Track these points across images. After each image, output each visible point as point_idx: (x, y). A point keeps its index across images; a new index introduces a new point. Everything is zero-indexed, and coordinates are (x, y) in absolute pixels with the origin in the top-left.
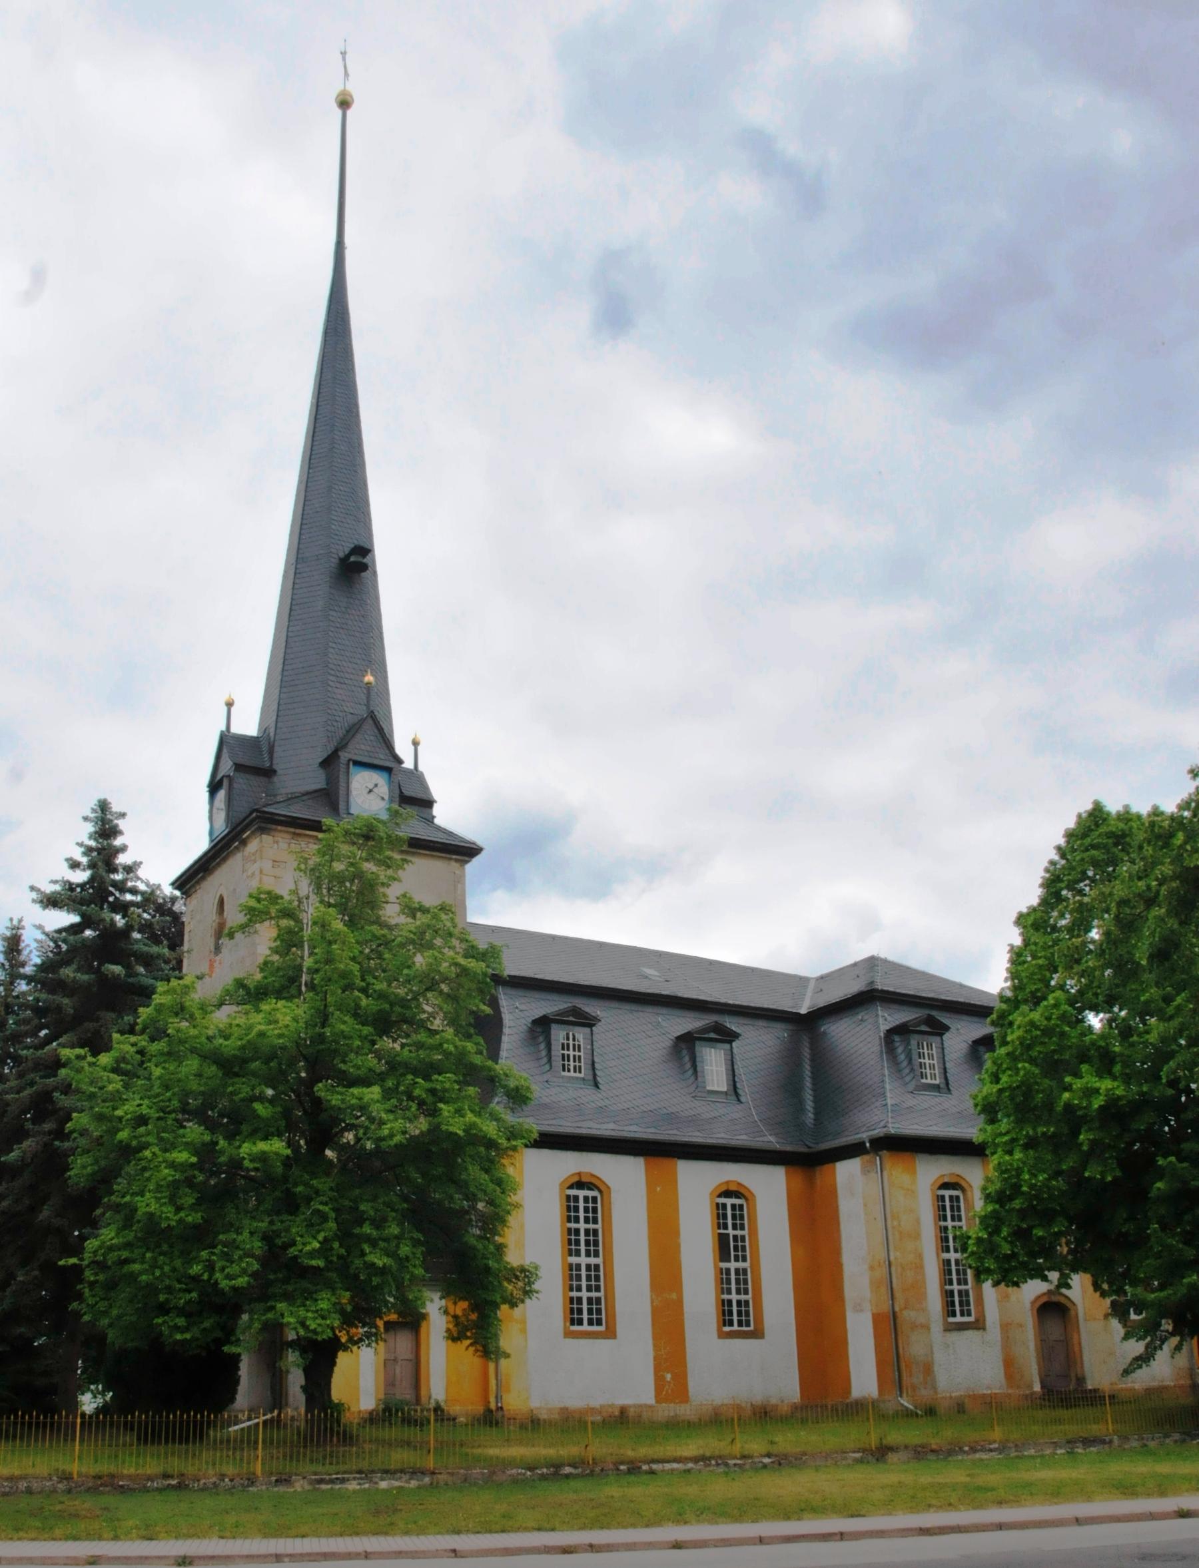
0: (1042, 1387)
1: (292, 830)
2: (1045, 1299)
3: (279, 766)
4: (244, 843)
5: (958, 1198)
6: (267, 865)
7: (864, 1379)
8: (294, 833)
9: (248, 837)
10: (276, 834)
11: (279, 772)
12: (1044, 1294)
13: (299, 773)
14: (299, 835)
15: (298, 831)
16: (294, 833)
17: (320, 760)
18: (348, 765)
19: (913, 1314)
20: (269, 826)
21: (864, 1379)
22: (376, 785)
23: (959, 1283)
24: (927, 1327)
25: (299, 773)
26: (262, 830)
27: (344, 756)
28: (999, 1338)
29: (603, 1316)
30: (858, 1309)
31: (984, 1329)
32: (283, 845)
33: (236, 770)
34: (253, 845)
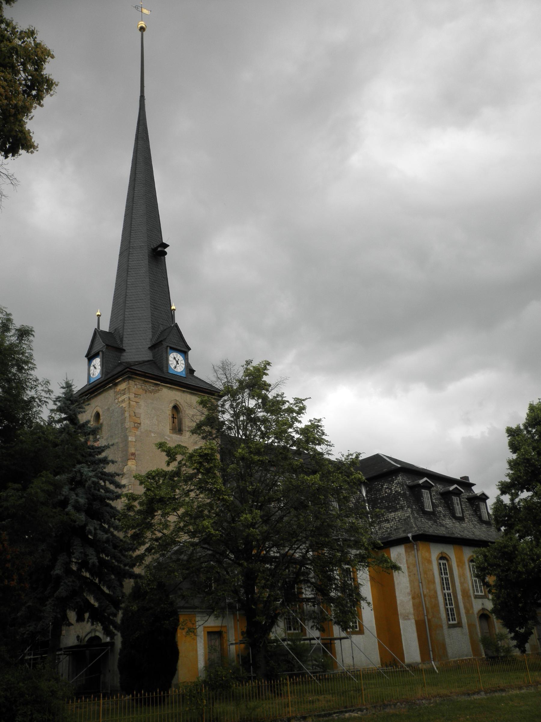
0: (486, 655)
1: (143, 379)
2: (481, 612)
3: (125, 346)
4: (116, 385)
5: (445, 564)
6: (132, 396)
7: (412, 651)
8: (144, 381)
9: (119, 382)
10: (136, 380)
11: (127, 351)
12: (481, 610)
13: (137, 350)
14: (146, 382)
15: (146, 380)
16: (144, 381)
17: (150, 346)
18: (167, 349)
19: (305, 605)
20: (133, 376)
21: (412, 651)
22: (175, 358)
23: (450, 605)
24: (441, 627)
25: (137, 350)
26: (130, 378)
27: (165, 344)
28: (468, 631)
29: (358, 624)
30: (406, 618)
31: (462, 627)
32: (139, 386)
33: (106, 348)
34: (123, 386)
